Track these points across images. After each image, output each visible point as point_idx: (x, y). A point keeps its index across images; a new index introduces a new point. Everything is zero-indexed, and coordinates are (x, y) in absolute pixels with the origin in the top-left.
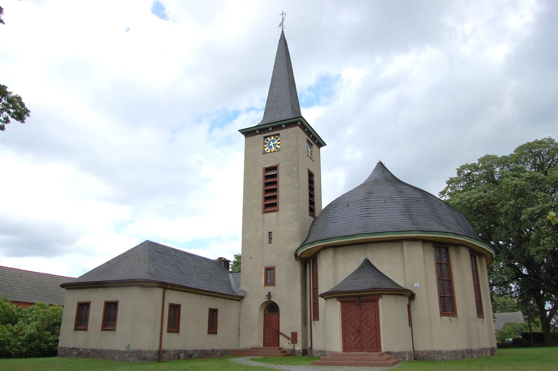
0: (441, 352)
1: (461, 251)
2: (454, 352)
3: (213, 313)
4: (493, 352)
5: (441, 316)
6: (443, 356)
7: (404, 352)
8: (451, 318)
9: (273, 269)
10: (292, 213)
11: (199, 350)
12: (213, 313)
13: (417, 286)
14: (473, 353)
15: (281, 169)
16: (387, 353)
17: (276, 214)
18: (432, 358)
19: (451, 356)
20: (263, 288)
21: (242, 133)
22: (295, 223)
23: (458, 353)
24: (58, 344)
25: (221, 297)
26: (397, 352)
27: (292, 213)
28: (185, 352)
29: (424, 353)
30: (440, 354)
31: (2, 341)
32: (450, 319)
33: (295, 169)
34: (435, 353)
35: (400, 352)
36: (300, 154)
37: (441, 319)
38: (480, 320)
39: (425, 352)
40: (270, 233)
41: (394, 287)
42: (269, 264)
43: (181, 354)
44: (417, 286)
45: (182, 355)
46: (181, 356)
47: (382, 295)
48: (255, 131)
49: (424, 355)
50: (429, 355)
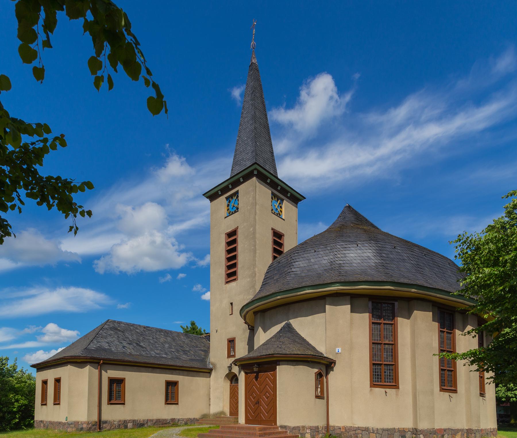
0: (367, 430)
1: (469, 319)
2: (388, 430)
3: (171, 386)
4: (470, 435)
5: (371, 387)
6: (371, 434)
7: (303, 427)
8: (451, 394)
9: (233, 340)
10: (249, 280)
11: (153, 420)
12: (171, 386)
13: (338, 351)
14: (418, 433)
15: (240, 232)
16: (282, 427)
17: (236, 283)
18: (351, 435)
19: (382, 435)
20: (226, 359)
21: (207, 198)
22: (251, 291)
23: (395, 432)
24: (311, 428)
25: (124, 364)
26: (293, 426)
27: (249, 280)
28: (134, 421)
29: (342, 429)
30: (367, 431)
31: (1, 407)
32: (450, 396)
33: (251, 229)
34: (359, 429)
35: (298, 426)
36: (257, 211)
37: (371, 390)
38: (482, 398)
39: (343, 429)
40: (232, 304)
41: (310, 353)
42: (230, 336)
43: (129, 424)
44: (338, 351)
45: (130, 425)
46: (128, 426)
47: (279, 362)
48: (217, 193)
49: (342, 432)
50: (348, 432)
